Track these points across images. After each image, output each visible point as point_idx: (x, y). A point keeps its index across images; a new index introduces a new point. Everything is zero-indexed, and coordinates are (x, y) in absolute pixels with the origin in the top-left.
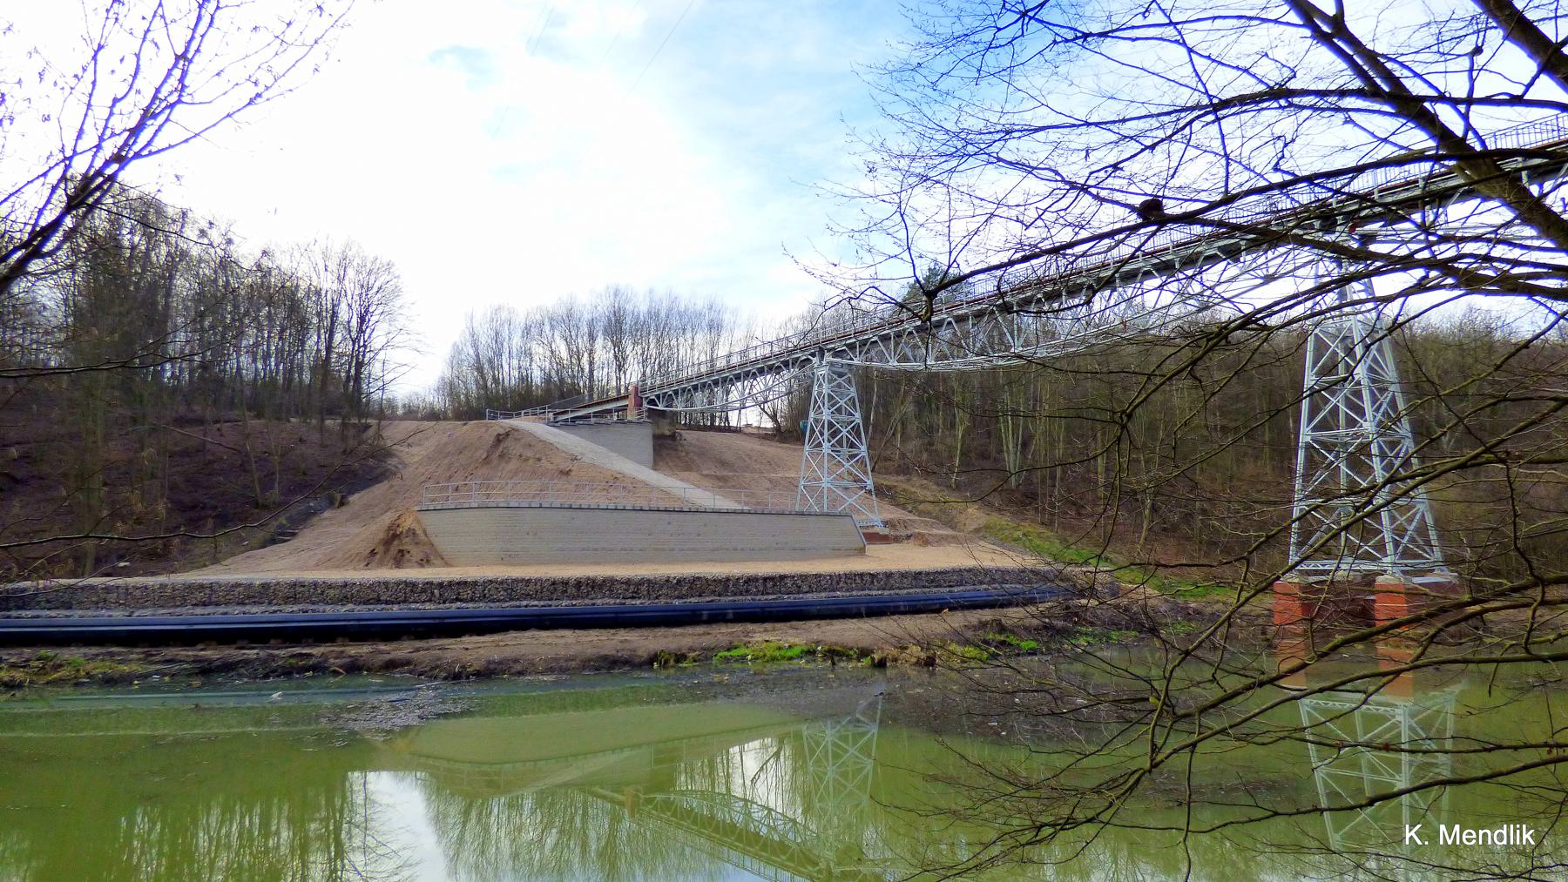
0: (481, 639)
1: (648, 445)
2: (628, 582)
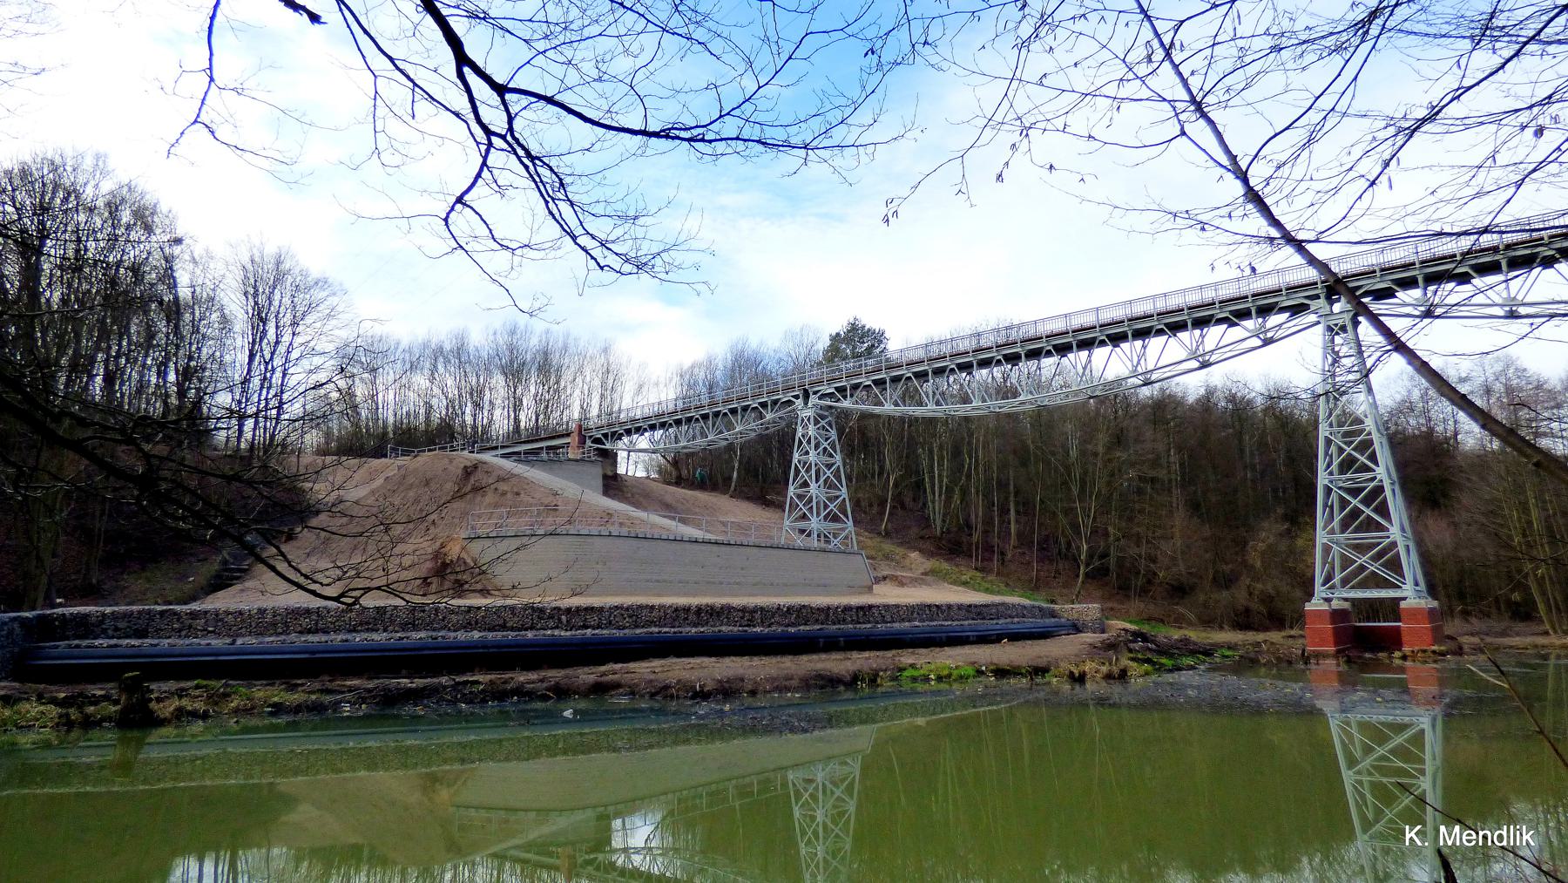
0: (691, 660)
1: (600, 482)
2: (744, 610)
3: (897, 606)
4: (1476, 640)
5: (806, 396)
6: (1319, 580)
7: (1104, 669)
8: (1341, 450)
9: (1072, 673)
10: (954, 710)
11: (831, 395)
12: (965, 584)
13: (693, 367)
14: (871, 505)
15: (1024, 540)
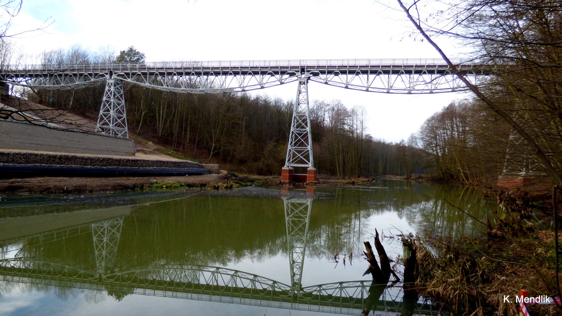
2: (83, 158)
3: (148, 161)
4: (323, 180)
5: (111, 74)
6: (287, 160)
7: (225, 185)
8: (298, 121)
9: (215, 186)
10: (166, 199)
11: (122, 76)
12: (169, 155)
13: (51, 52)
14: (133, 122)
15: (192, 141)
